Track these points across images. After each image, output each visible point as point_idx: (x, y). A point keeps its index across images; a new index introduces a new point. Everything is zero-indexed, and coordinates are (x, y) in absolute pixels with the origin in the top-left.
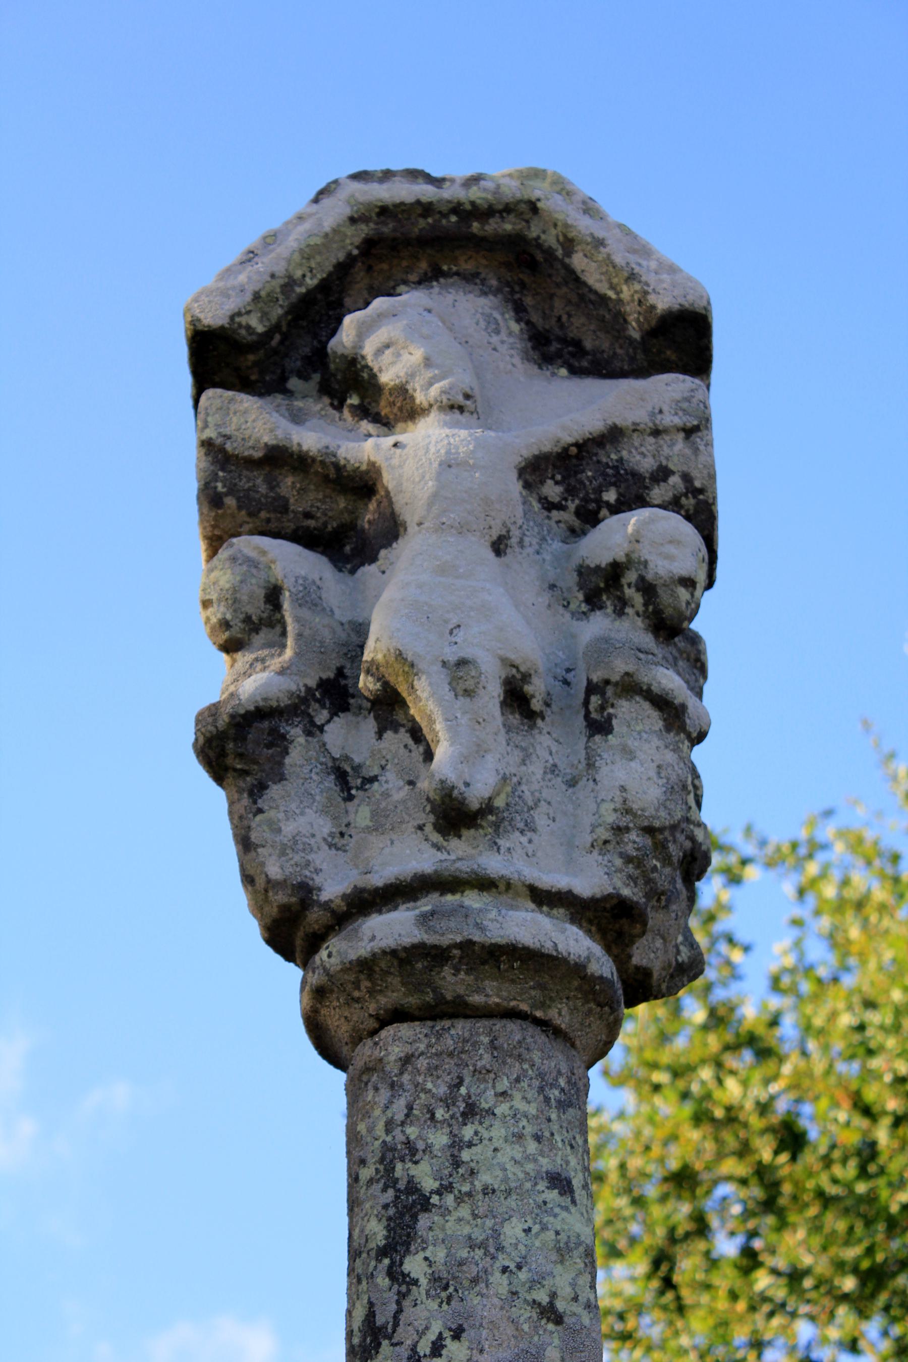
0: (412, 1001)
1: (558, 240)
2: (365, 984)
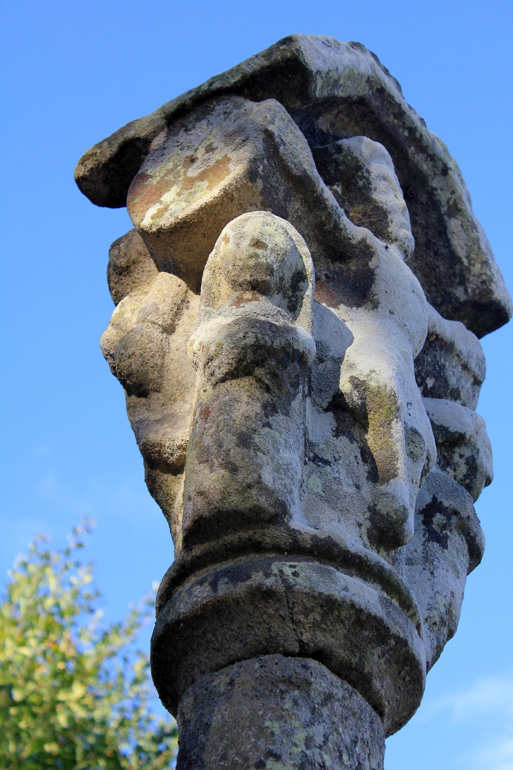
0: (342, 654)
1: (448, 202)
2: (315, 616)
